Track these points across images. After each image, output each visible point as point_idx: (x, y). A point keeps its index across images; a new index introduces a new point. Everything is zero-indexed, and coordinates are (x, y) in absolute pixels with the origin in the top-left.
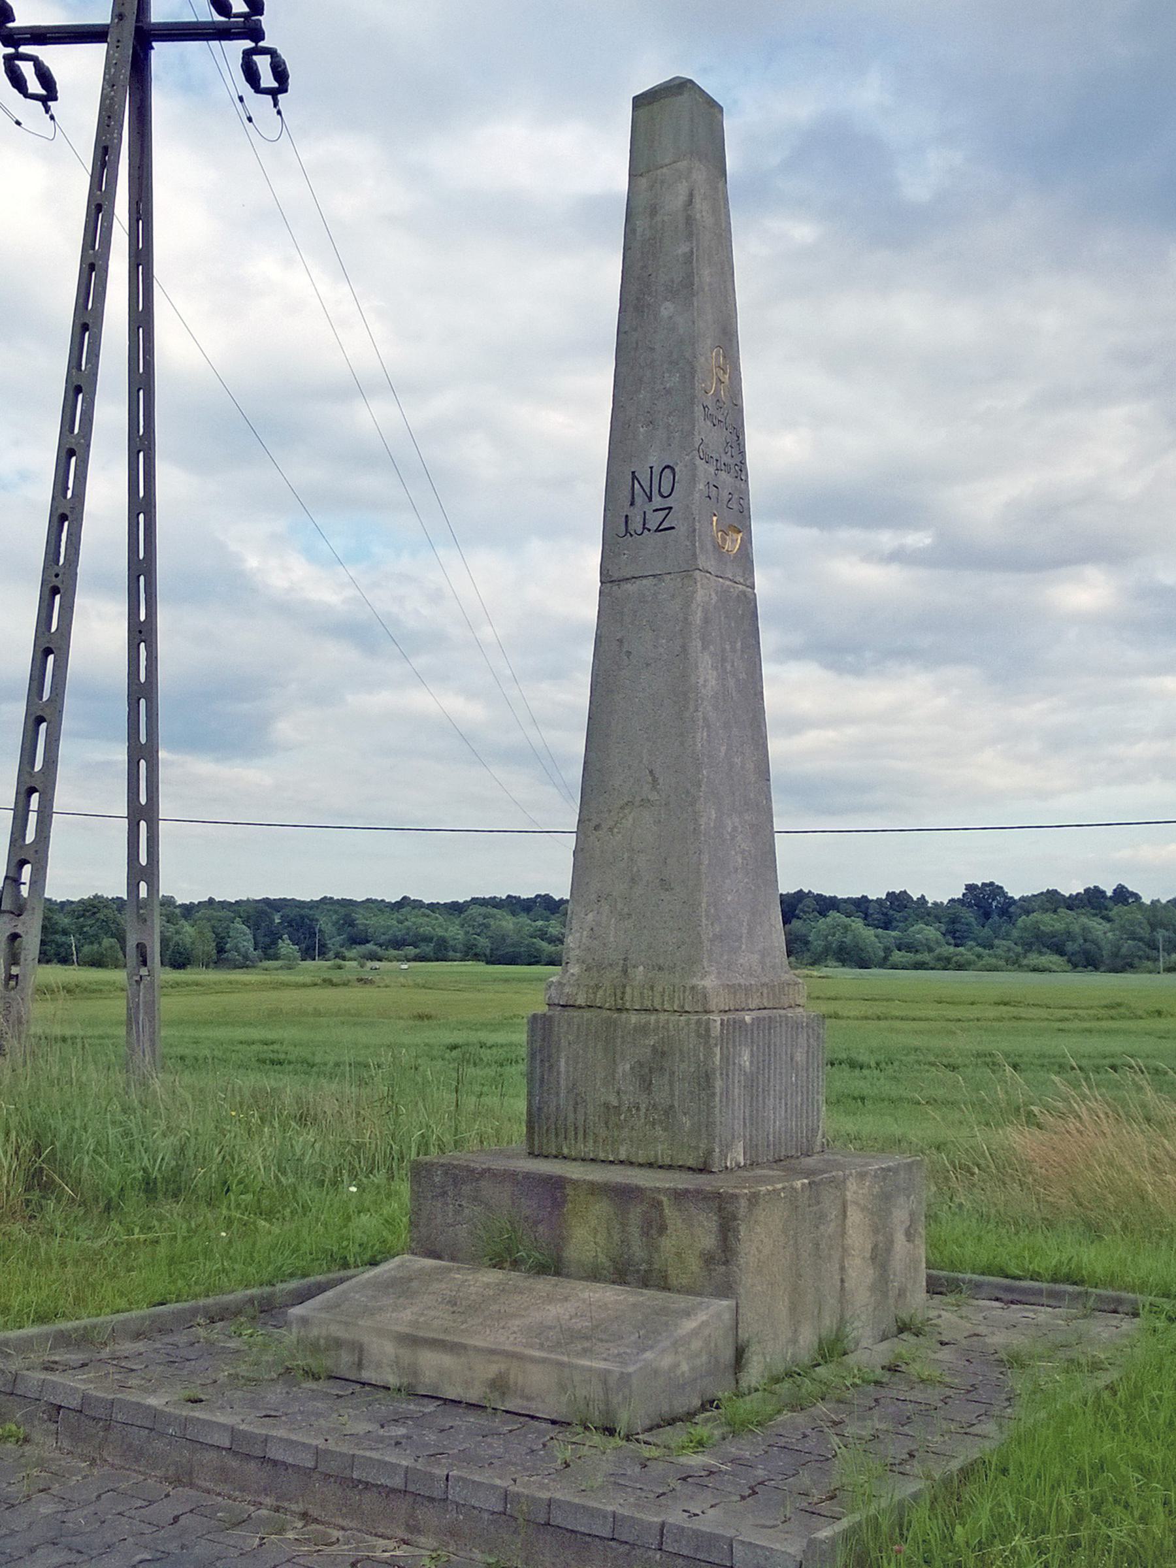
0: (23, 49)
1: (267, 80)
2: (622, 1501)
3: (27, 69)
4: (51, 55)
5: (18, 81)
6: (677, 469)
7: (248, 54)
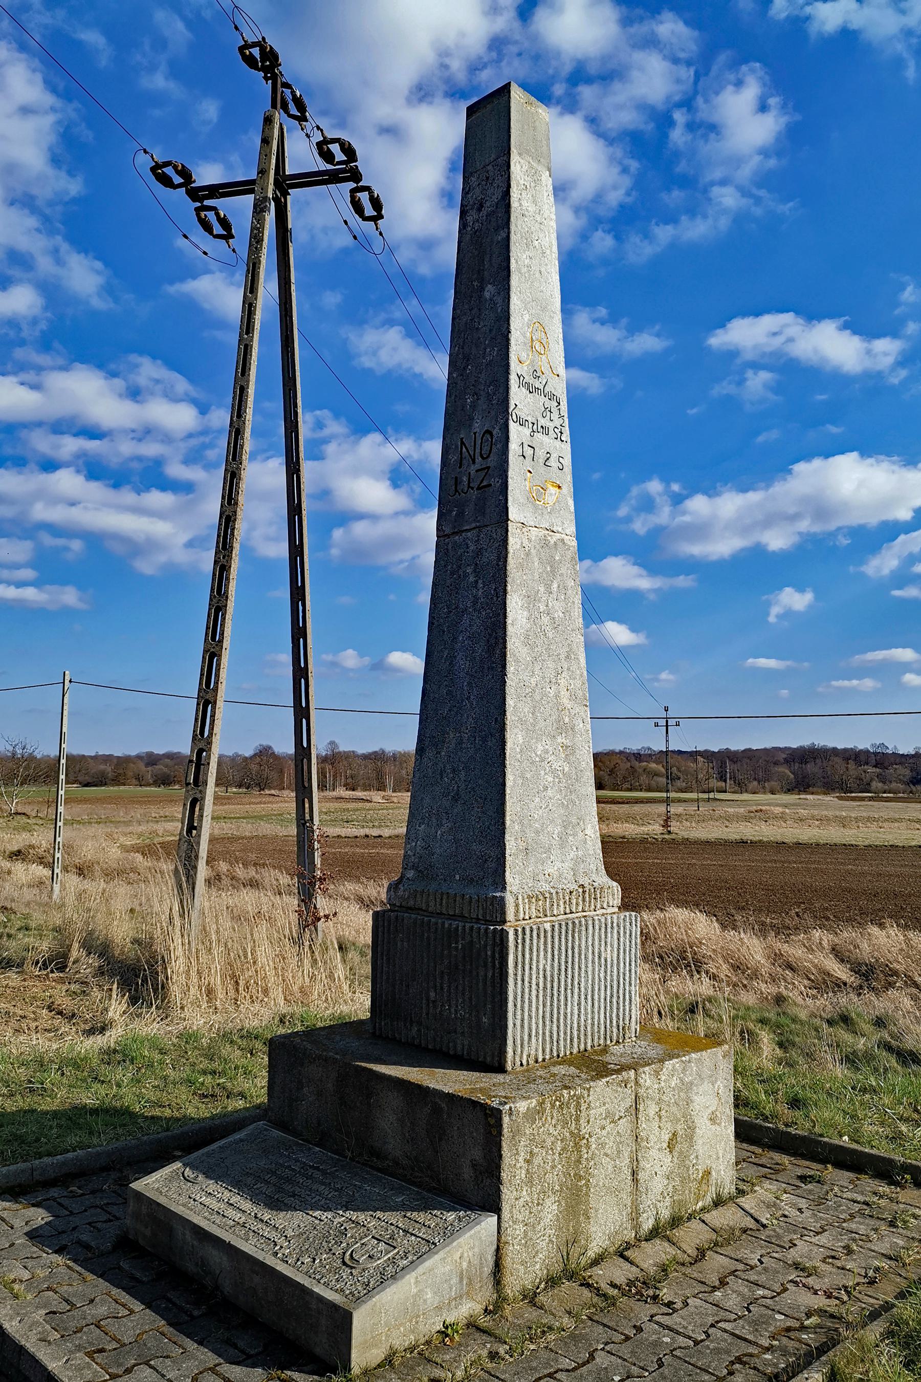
0: (207, 203)
1: (369, 211)
2: (769, 1216)
3: (211, 216)
4: (224, 205)
5: (207, 227)
6: (494, 433)
7: (353, 191)
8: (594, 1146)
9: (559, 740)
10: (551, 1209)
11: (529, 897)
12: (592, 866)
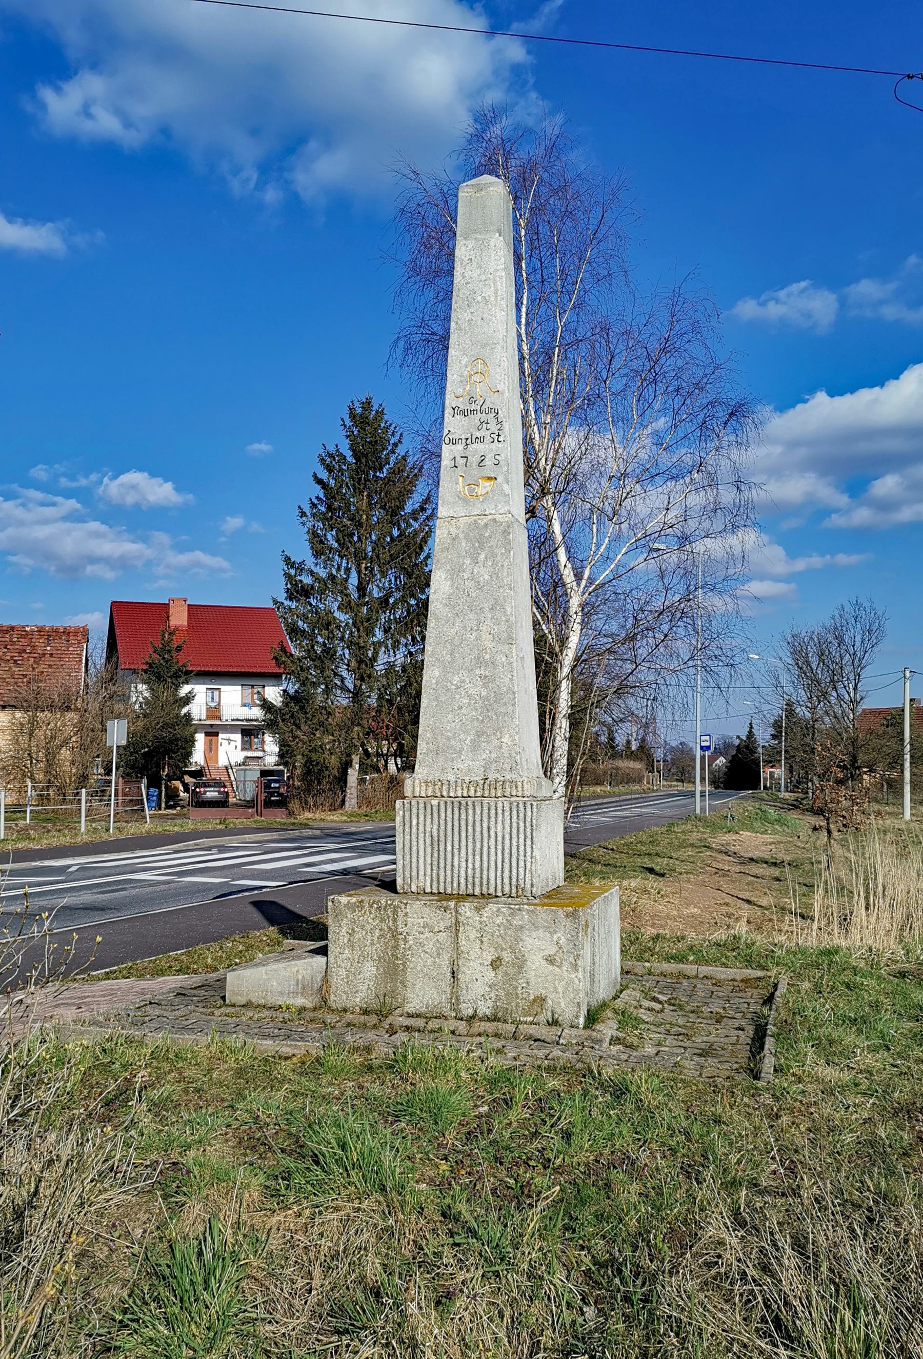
8: (411, 942)
9: (478, 672)
10: (370, 969)
11: (426, 782)
12: (506, 765)
